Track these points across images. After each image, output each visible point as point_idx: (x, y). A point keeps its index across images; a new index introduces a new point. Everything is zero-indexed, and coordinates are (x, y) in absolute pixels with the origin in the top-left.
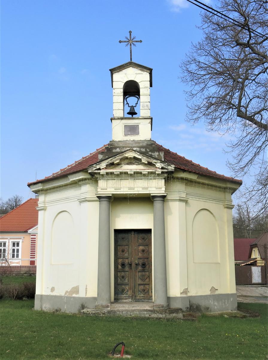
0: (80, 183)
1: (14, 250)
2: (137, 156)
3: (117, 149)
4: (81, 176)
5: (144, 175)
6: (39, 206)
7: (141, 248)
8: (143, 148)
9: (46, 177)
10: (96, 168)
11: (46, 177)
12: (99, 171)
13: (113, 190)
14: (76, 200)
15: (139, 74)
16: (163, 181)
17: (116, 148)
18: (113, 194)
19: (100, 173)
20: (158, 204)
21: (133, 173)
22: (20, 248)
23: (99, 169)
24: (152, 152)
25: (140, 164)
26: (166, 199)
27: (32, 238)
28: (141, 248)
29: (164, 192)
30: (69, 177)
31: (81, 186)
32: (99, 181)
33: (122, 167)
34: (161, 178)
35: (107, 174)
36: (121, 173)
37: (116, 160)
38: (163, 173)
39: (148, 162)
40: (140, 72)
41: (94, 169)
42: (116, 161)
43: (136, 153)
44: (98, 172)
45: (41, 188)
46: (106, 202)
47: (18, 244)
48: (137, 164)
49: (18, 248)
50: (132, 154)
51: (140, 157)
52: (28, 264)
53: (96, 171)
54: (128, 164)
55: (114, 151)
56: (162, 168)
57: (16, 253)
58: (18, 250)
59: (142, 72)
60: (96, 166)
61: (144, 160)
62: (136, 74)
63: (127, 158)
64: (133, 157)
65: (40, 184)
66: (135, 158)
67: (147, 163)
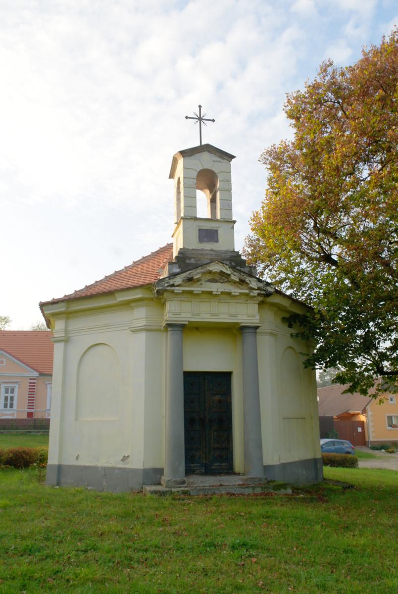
0: (132, 305)
1: (6, 398)
2: (224, 270)
3: (192, 260)
4: (138, 295)
5: (235, 296)
6: (55, 336)
7: (217, 398)
8: (227, 261)
9: (53, 299)
10: (168, 284)
11: (53, 299)
12: (173, 288)
13: (189, 315)
14: (127, 328)
15: (217, 161)
16: (257, 306)
17: (190, 258)
18: (190, 322)
19: (173, 290)
20: (249, 338)
21: (219, 293)
22: (16, 395)
23: (173, 285)
24: (241, 267)
25: (226, 282)
26: (258, 330)
27: (30, 383)
28: (217, 398)
29: (258, 321)
30: (117, 295)
31: (133, 309)
32: (168, 304)
33: (201, 284)
34: (254, 302)
35: (184, 292)
36: (203, 292)
37: (196, 274)
38: (259, 294)
39: (240, 279)
40: (219, 159)
41: (166, 285)
42: (196, 275)
43: (224, 266)
44: (172, 289)
45: (64, 309)
46: (179, 332)
47: (12, 391)
48: (222, 281)
49: (6, 395)
50: (217, 268)
51: (229, 272)
52: (25, 416)
53: (169, 288)
54: (210, 281)
55: (187, 261)
56: (259, 289)
57: (9, 402)
58: (12, 398)
59: (222, 160)
60: (169, 281)
61: (235, 277)
62: (214, 161)
63: (210, 272)
64: (218, 271)
65: (63, 304)
66: (222, 273)
67: (238, 280)
